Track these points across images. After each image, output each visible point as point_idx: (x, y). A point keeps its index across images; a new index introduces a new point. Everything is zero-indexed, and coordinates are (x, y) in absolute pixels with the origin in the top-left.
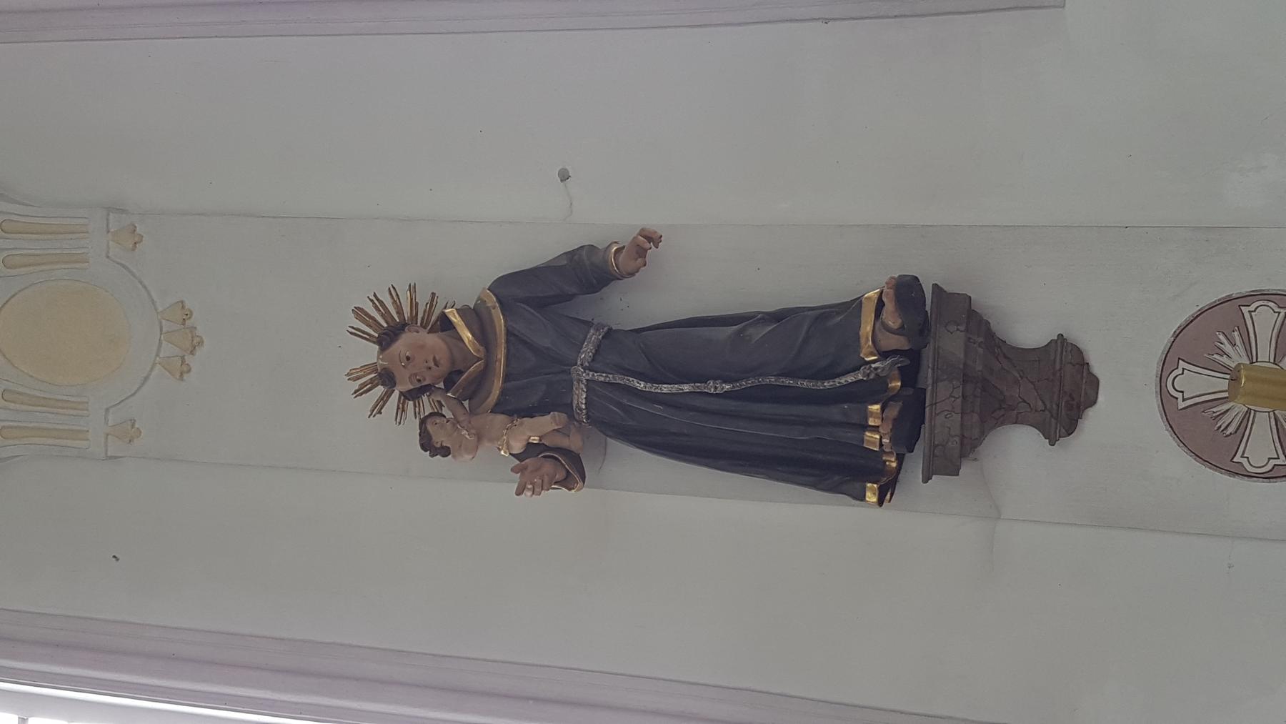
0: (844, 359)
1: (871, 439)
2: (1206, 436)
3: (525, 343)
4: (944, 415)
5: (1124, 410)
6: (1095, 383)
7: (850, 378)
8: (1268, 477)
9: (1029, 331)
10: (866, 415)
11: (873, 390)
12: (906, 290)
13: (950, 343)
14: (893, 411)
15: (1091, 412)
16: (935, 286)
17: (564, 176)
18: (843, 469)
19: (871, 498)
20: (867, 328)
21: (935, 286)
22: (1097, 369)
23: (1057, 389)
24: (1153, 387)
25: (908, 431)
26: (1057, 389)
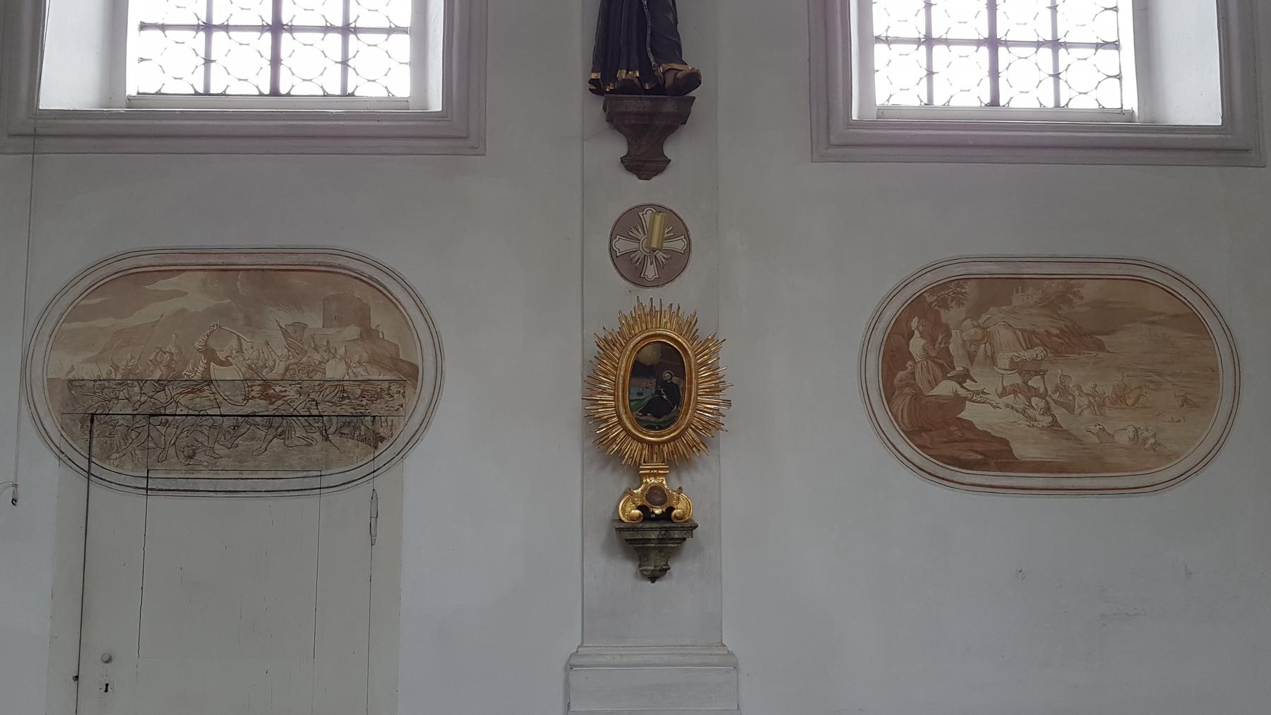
0: (661, 60)
1: (622, 74)
2: (628, 223)
3: (1061, 469)
4: (633, 104)
5: (637, 191)
6: (648, 178)
7: (652, 59)
8: (611, 248)
9: (669, 150)
10: (634, 70)
11: (647, 72)
12: (694, 80)
13: (669, 106)
14: (636, 81)
15: (635, 177)
16: (694, 98)
17: (14, 501)
18: (607, 56)
19: (594, 76)
20: (676, 66)
21: (694, 98)
22: (654, 179)
23: (645, 162)
24: (648, 202)
25: (627, 89)
26: (645, 162)
